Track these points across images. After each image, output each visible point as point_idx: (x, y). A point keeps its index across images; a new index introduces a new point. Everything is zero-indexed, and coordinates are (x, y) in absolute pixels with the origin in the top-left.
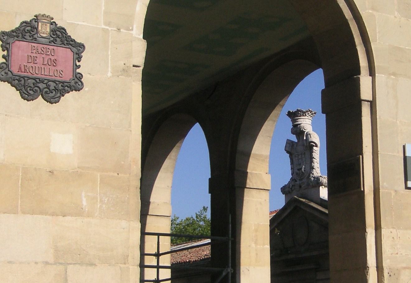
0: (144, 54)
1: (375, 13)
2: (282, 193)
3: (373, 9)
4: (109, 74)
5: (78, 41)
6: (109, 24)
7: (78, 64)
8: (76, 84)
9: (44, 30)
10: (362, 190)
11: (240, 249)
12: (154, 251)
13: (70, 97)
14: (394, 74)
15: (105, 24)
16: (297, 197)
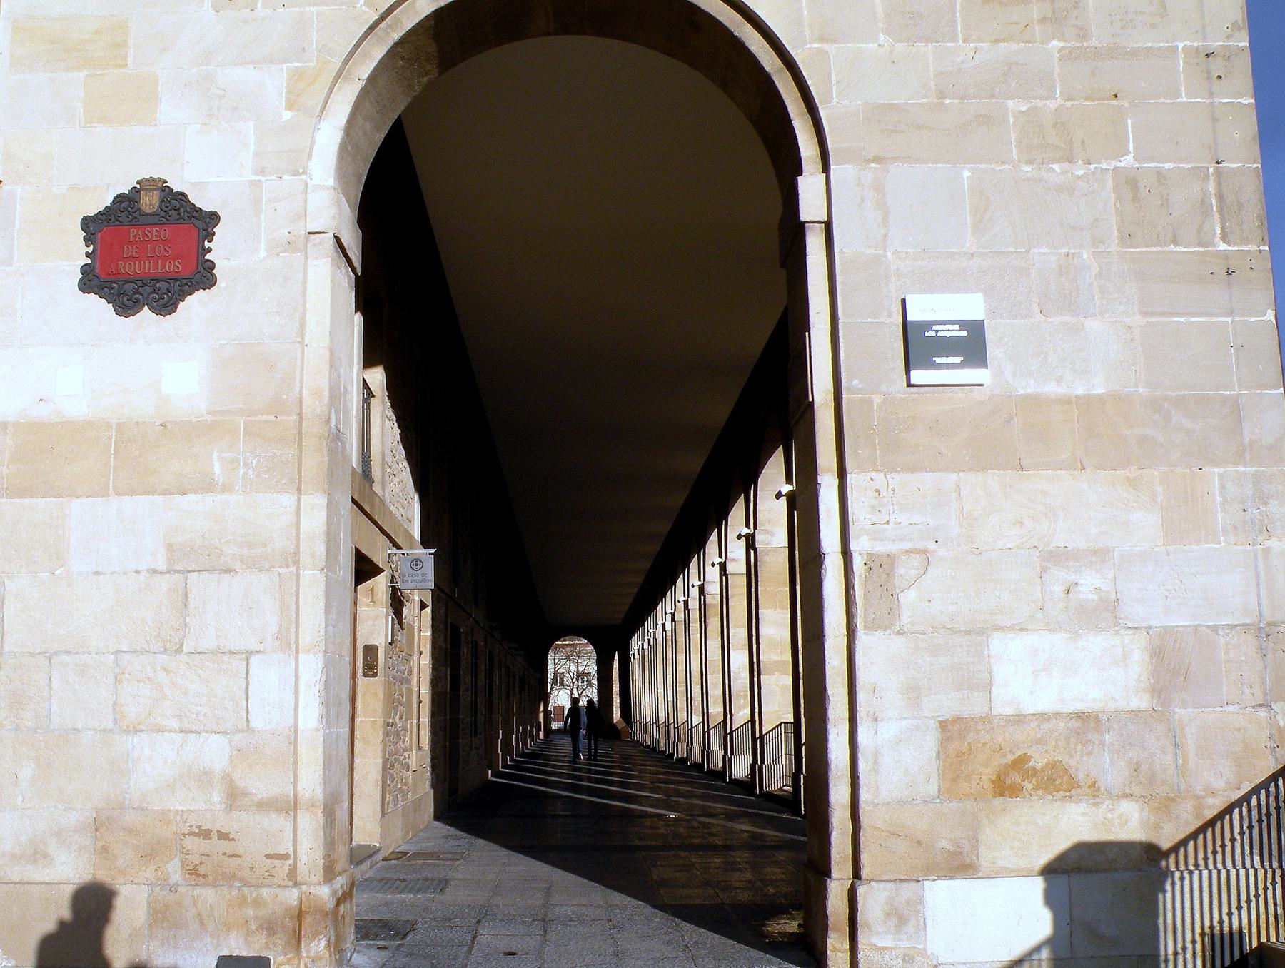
1: (826, 47)
2: (85, 270)
3: (822, 39)
4: (263, 254)
6: (262, 172)
7: (207, 244)
8: (203, 277)
9: (150, 202)
13: (194, 303)
14: (877, 159)
15: (256, 173)
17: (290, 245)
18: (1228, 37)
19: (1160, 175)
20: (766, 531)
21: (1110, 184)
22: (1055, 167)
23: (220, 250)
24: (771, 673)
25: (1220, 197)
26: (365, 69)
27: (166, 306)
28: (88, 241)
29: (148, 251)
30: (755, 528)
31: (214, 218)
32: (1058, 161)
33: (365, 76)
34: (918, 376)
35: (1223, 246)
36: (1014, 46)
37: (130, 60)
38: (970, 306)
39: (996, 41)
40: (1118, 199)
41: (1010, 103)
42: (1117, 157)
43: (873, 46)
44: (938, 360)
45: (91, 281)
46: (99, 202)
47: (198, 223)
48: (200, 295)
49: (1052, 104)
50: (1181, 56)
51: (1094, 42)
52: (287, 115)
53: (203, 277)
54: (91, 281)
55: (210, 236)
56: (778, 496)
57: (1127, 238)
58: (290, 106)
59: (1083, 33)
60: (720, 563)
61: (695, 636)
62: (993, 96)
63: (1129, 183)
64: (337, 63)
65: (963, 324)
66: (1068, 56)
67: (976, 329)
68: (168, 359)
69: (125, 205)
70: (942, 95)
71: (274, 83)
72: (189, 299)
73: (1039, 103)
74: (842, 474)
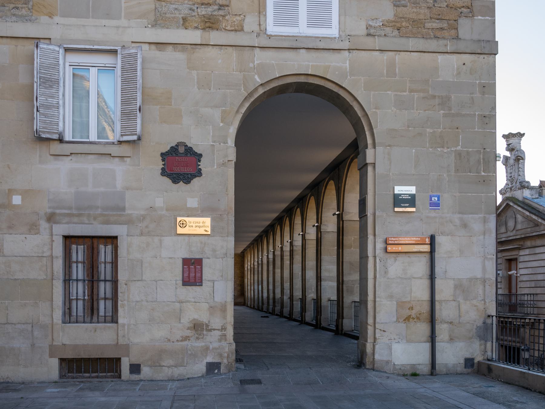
0: (235, 154)
1: (377, 111)
2: (163, 169)
3: (376, 108)
4: (215, 167)
5: (199, 152)
6: (214, 142)
7: (199, 163)
8: (199, 173)
9: (182, 150)
10: (402, 205)
11: (235, 289)
12: (107, 301)
13: (196, 181)
14: (389, 146)
15: (213, 142)
16: (482, 16)
17: (223, 164)
18: (490, 112)
19: (468, 152)
20: (325, 225)
21: (453, 154)
22: (439, 149)
23: (203, 165)
24: (325, 280)
25: (484, 159)
28: (163, 160)
29: (181, 164)
30: (321, 223)
31: (201, 155)
32: (440, 148)
33: (243, 112)
34: (396, 209)
35: (483, 174)
36: (430, 112)
37: (173, 103)
38: (412, 190)
39: (425, 110)
40: (455, 159)
41: (428, 130)
42: (456, 147)
43: (390, 111)
44: (402, 205)
45: (164, 173)
47: (196, 157)
48: (197, 178)
49: (439, 130)
50: (477, 116)
51: (453, 112)
52: (221, 124)
53: (199, 173)
54: (164, 173)
55: (200, 161)
56: (334, 214)
57: (457, 171)
58: (222, 122)
59: (450, 109)
60: (302, 235)
61: (287, 262)
62: (423, 127)
63: (459, 154)
64: (236, 109)
65: (410, 195)
66: (445, 115)
67: (413, 196)
69: (174, 150)
70: (408, 127)
71: (217, 114)
72: (194, 180)
73: (436, 130)
74: (375, 235)
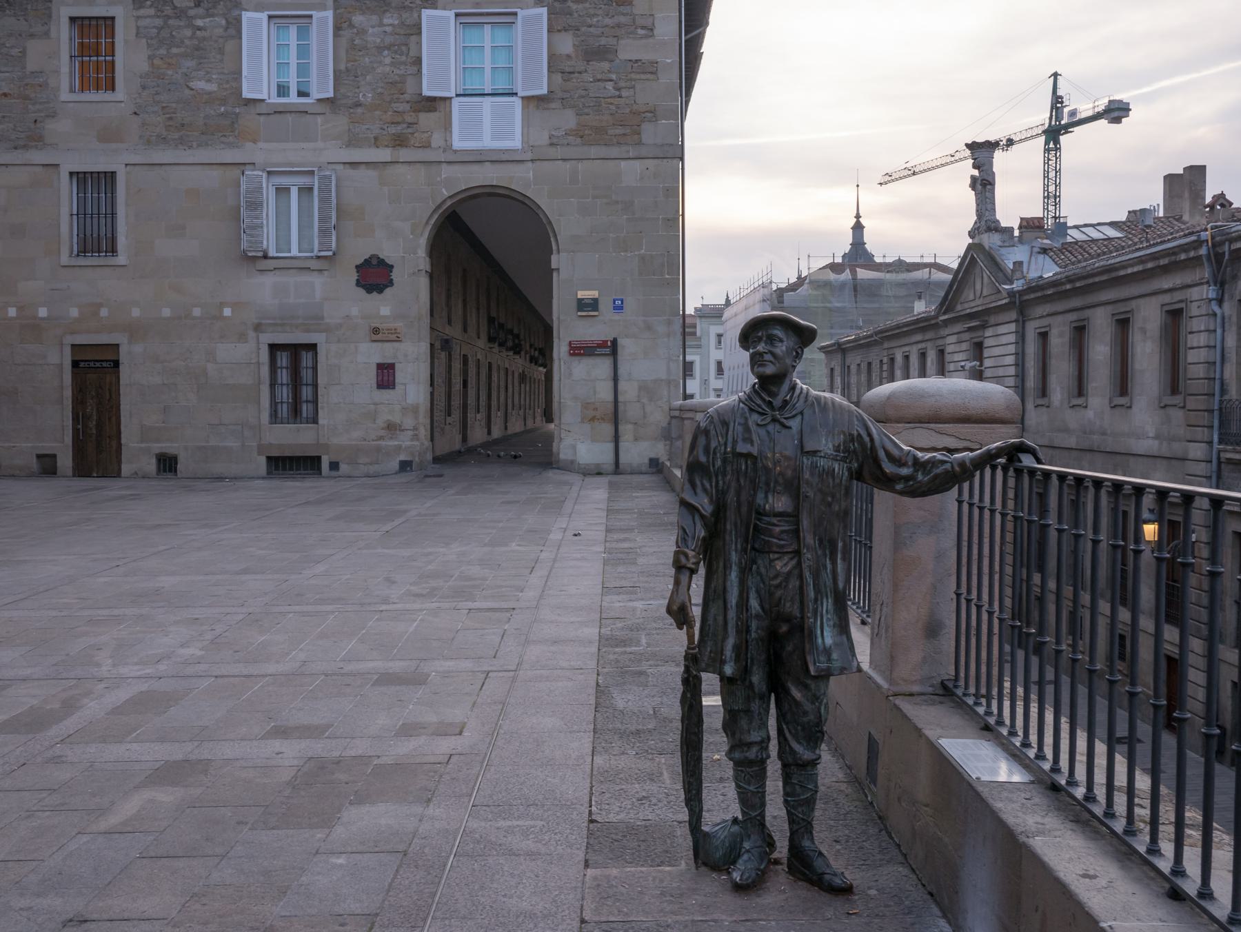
8: (358, 268)
9: (374, 262)
13: (388, 291)
26: (432, 222)
27: (381, 291)
29: (374, 275)
31: (392, 267)
38: (594, 294)
45: (358, 284)
46: (360, 261)
53: (390, 283)
54: (358, 284)
67: (596, 301)
68: (383, 307)
69: (367, 262)
